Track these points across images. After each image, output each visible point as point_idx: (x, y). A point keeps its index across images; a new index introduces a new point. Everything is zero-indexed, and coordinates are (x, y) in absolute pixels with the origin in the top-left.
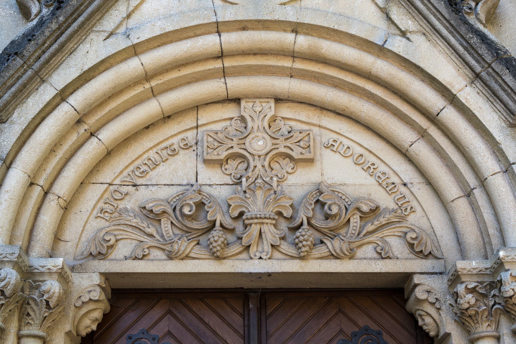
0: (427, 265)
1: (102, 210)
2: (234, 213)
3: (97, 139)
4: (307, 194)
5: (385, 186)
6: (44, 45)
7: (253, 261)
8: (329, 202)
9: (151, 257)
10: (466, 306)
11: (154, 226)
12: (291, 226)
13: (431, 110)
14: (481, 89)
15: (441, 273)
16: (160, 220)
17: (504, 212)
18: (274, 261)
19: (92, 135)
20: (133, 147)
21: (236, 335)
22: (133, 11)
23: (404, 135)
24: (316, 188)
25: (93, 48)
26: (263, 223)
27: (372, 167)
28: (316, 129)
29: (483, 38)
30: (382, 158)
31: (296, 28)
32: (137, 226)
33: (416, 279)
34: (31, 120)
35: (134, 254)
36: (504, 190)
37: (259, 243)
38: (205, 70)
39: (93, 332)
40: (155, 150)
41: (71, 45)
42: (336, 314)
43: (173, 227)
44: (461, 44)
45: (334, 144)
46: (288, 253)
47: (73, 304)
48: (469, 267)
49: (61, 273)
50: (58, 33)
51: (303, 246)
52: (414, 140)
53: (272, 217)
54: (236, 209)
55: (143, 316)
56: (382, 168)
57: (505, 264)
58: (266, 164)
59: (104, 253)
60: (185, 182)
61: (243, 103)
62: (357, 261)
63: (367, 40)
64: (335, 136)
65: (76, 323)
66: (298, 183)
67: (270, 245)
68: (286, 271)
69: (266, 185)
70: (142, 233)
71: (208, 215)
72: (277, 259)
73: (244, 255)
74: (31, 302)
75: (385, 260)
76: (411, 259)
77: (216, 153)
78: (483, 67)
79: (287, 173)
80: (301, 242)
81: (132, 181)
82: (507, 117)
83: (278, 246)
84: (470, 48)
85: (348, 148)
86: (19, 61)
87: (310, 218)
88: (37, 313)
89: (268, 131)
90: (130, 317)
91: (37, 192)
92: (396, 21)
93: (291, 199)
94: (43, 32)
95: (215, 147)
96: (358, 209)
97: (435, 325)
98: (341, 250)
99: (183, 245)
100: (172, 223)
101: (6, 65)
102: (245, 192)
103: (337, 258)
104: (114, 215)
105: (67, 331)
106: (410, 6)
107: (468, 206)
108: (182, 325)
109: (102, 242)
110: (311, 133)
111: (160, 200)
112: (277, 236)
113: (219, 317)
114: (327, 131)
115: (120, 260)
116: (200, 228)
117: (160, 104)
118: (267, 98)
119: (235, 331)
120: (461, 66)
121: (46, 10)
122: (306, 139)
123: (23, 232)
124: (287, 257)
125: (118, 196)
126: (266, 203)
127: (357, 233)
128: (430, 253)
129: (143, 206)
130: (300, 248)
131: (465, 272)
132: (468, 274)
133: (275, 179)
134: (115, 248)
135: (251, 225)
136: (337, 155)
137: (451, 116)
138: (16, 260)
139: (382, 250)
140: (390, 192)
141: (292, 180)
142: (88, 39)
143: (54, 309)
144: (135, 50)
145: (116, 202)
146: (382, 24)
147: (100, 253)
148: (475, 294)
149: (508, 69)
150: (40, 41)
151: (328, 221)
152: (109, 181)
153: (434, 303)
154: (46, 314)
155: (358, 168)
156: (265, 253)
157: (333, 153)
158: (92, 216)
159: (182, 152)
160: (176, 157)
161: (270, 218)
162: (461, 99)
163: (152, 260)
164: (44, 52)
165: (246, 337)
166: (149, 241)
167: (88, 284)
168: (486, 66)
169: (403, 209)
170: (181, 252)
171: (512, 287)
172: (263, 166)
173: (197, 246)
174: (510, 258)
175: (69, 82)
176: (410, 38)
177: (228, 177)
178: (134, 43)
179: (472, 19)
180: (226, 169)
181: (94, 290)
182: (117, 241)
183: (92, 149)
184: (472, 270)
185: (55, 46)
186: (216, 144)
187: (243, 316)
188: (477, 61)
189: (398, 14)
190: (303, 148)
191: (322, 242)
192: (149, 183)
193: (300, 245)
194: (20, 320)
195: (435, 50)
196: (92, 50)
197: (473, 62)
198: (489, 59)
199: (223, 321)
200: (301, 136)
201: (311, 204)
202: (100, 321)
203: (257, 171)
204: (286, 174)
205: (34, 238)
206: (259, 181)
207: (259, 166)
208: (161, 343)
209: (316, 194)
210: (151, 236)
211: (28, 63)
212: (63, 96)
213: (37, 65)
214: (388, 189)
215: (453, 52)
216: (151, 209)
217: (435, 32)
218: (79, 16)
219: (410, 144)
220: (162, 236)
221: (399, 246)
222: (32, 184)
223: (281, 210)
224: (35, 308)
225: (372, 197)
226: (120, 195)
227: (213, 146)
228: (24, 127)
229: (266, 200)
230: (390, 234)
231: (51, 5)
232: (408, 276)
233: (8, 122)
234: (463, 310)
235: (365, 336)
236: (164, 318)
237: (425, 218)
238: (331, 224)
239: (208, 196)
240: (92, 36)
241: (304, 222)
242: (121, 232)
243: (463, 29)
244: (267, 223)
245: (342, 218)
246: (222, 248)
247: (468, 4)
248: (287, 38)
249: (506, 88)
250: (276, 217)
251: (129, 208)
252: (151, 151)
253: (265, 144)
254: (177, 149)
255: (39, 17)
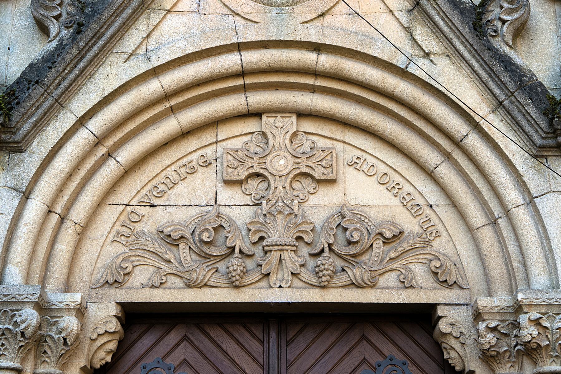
0: (451, 295)
1: (118, 234)
2: (254, 238)
3: (115, 161)
4: (328, 219)
5: (410, 209)
6: (64, 71)
7: (272, 289)
8: (351, 228)
9: (168, 285)
10: (488, 346)
11: (172, 251)
12: (312, 252)
13: (455, 136)
14: (505, 117)
15: (467, 305)
16: (178, 245)
17: (527, 247)
18: (294, 290)
19: (109, 155)
20: (150, 165)
21: (255, 364)
22: (153, 30)
23: (430, 157)
24: (338, 209)
25: (113, 72)
26: (283, 250)
27: (397, 187)
28: (339, 145)
29: (508, 64)
30: (407, 178)
31: (318, 48)
32: (154, 251)
33: (440, 311)
34: (50, 149)
35: (151, 282)
36: (527, 224)
37: (279, 270)
38: (226, 88)
39: (107, 363)
40: (173, 168)
41: (91, 69)
42: (360, 341)
43: (191, 252)
44: (484, 69)
45: (357, 161)
46: (308, 282)
47: (89, 336)
48: (491, 305)
49: (79, 309)
50: (78, 57)
51: (324, 275)
52: (438, 163)
53: (292, 243)
54: (255, 234)
55: (158, 343)
56: (407, 188)
57: (524, 307)
58: (287, 185)
59: (121, 281)
60: (204, 203)
61: (264, 117)
62: (379, 290)
63: (389, 62)
64: (359, 153)
65: (91, 356)
66: (320, 206)
67: (290, 273)
68: (306, 301)
69: (287, 209)
70: (160, 259)
71: (228, 241)
72: (297, 288)
73: (264, 283)
74: (48, 339)
75: (408, 290)
76: (435, 289)
77: (236, 173)
78: (506, 95)
79: (308, 192)
80: (322, 271)
81: (149, 201)
82: (531, 147)
83: (299, 274)
84: (492, 74)
85: (372, 165)
86: (41, 90)
87: (332, 244)
88: (53, 350)
89: (289, 149)
90: (146, 342)
91: (54, 218)
92: (419, 42)
93: (312, 223)
94: (63, 58)
95: (235, 166)
96: (381, 234)
97: (460, 360)
98: (363, 280)
99: (202, 273)
100: (190, 247)
101: (27, 94)
102: (265, 215)
103: (359, 287)
104: (130, 238)
105: (83, 366)
106: (435, 26)
107: (494, 235)
108: (199, 353)
109: (119, 270)
110: (333, 151)
111: (179, 224)
112: (297, 264)
113: (238, 344)
114: (351, 148)
115: (138, 289)
116: (219, 254)
117: (179, 122)
118: (290, 113)
119: (254, 359)
120: (485, 92)
121: (66, 32)
122: (329, 157)
123: (40, 264)
124: (308, 286)
125: (135, 218)
126: (287, 229)
127: (379, 260)
128: (455, 282)
129: (160, 229)
130: (320, 277)
131: (486, 310)
132: (489, 312)
133: (296, 202)
134: (132, 275)
135: (271, 251)
136: (361, 173)
137: (474, 142)
138: (37, 300)
139: (405, 278)
140: (415, 215)
141: (313, 200)
142: (108, 61)
143: (70, 346)
144: (155, 72)
145: (132, 224)
146: (406, 46)
147: (116, 281)
148: (497, 334)
149: (531, 99)
150: (61, 69)
151: (350, 247)
152: (127, 203)
153: (459, 337)
154: (63, 352)
155: (383, 187)
156: (285, 282)
157: (357, 171)
158: (108, 240)
159: (201, 170)
160: (194, 175)
161: (290, 245)
162: (484, 127)
163: (170, 289)
164: (64, 78)
165: (264, 366)
166: (166, 268)
167: (104, 314)
168: (510, 94)
169: (428, 234)
170: (199, 281)
171: (530, 332)
172: (284, 188)
173: (215, 274)
174: (529, 300)
175: (89, 109)
176: (434, 61)
177: (248, 197)
178: (155, 66)
179: (497, 43)
180: (246, 189)
181: (111, 322)
182: (134, 267)
183: (110, 170)
184: (493, 308)
185: (76, 72)
186: (236, 163)
187: (262, 342)
188: (501, 89)
189: (423, 35)
190: (325, 168)
191: (343, 270)
192: (166, 204)
193: (321, 274)
194: (36, 358)
195: (458, 74)
196: (112, 73)
197: (496, 90)
198: (512, 88)
199: (242, 349)
200: (323, 154)
201: (333, 229)
202: (115, 351)
203: (277, 193)
204: (307, 195)
205: (50, 268)
206: (280, 203)
207: (280, 188)
208: (177, 373)
209: (338, 217)
210: (169, 261)
211: (48, 91)
212: (82, 121)
213: (58, 92)
214: (413, 211)
215: (477, 77)
216: (169, 234)
217: (458, 55)
218: (99, 38)
219: (435, 166)
220: (180, 263)
221: (423, 274)
222: (50, 211)
223: (302, 235)
224: (52, 345)
225: (397, 220)
226: (137, 217)
227: (233, 166)
228: (44, 157)
229: (287, 225)
230: (414, 261)
231: (71, 27)
232: (433, 307)
233: (28, 151)
234: (485, 350)
235: (390, 366)
236: (180, 344)
237: (451, 243)
238: (353, 250)
239: (227, 219)
240: (112, 58)
241: (325, 249)
242: (138, 258)
243: (486, 55)
244: (287, 250)
245: (365, 243)
246: (241, 278)
247: (493, 25)
248: (309, 58)
249: (529, 118)
250: (296, 243)
251: (146, 231)
252: (169, 169)
253: (286, 162)
254: (196, 167)
255: (58, 38)
